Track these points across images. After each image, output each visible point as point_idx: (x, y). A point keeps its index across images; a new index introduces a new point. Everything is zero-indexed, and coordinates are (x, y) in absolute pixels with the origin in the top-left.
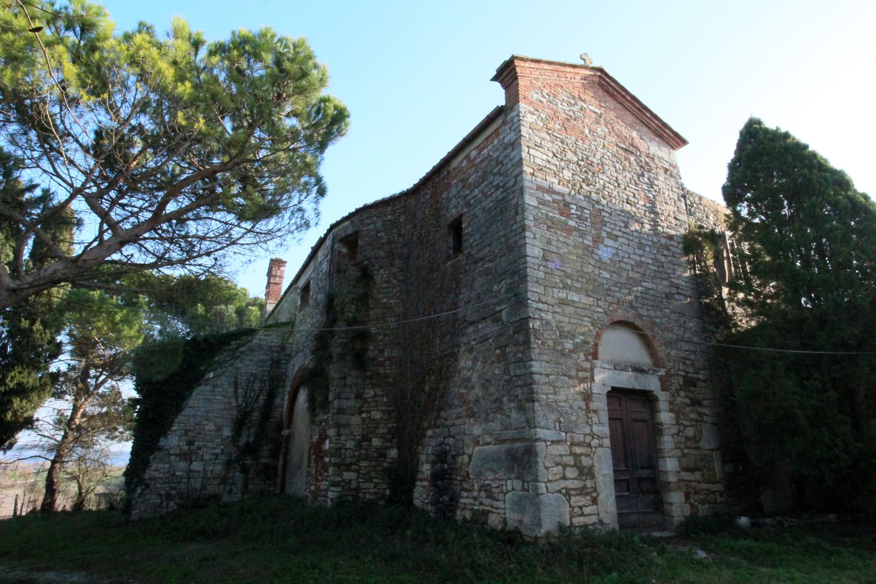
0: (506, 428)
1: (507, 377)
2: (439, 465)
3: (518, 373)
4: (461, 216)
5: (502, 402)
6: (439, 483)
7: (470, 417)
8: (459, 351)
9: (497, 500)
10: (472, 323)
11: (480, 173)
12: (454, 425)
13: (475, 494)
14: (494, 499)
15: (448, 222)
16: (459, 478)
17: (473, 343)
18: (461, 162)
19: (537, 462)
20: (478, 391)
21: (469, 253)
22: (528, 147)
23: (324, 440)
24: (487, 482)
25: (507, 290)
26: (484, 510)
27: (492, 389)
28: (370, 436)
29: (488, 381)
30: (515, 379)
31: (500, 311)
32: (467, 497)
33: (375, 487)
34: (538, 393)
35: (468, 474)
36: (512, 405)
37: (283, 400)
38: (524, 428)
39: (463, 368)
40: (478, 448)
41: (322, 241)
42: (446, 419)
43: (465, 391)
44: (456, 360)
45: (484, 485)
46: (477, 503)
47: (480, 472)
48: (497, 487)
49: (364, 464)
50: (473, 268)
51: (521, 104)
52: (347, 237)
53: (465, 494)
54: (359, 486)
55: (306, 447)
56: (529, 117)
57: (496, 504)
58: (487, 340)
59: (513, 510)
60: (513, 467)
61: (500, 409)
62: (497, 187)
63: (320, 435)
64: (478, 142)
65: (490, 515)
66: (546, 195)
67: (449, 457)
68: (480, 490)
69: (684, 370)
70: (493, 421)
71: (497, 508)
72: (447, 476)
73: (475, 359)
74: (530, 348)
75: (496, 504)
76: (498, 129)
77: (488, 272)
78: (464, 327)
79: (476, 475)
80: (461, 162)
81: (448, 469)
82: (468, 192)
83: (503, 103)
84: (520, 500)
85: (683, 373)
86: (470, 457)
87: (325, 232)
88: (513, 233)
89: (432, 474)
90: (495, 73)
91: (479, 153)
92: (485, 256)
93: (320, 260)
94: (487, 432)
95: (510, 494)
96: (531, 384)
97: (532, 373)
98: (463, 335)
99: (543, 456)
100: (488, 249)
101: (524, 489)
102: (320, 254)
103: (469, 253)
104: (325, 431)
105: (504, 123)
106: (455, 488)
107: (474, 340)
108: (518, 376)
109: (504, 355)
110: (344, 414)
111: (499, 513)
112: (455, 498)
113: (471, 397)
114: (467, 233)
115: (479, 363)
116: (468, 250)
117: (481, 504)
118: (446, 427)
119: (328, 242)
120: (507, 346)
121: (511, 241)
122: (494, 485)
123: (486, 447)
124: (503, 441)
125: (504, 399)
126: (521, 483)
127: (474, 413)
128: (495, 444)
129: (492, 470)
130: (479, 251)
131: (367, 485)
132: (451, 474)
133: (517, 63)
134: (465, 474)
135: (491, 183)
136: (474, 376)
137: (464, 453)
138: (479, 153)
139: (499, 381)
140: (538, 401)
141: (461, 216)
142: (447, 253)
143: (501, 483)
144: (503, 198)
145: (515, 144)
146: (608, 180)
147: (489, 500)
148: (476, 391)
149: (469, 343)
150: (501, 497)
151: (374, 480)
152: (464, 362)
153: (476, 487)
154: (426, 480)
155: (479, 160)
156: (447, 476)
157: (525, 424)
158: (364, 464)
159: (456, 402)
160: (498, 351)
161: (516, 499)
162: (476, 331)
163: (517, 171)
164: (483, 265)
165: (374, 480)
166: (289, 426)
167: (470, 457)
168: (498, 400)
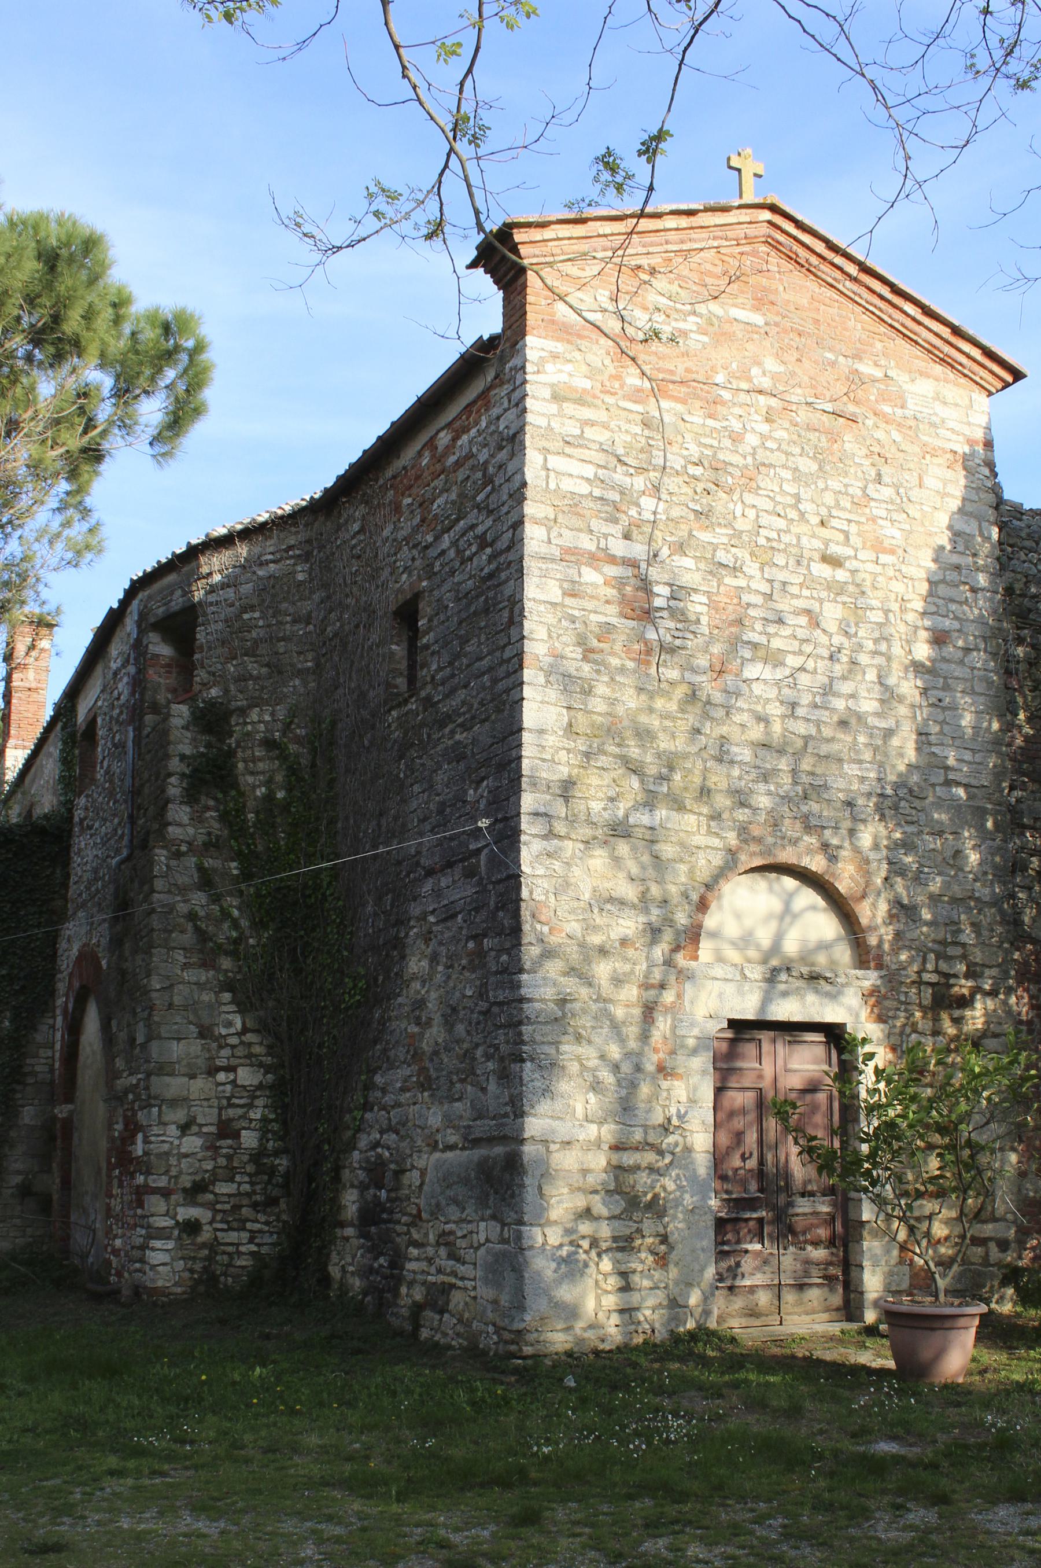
0: (480, 1117)
1: (483, 1005)
2: (372, 1191)
3: (501, 998)
4: (417, 596)
5: (474, 1059)
6: (373, 1229)
7: (422, 1087)
8: (407, 935)
9: (464, 1263)
10: (430, 873)
11: (453, 496)
12: (398, 1105)
13: (430, 1251)
14: (458, 1260)
15: (393, 607)
16: (404, 1219)
17: (432, 919)
18: (420, 454)
19: (522, 1186)
20: (436, 1033)
21: (428, 699)
22: (545, 451)
23: (133, 1136)
24: (448, 1227)
25: (489, 803)
26: (443, 1283)
27: (460, 1028)
28: (236, 1125)
29: (454, 1010)
30: (495, 1009)
31: (479, 851)
32: (417, 1259)
33: (251, 1241)
34: (534, 1042)
35: (419, 1211)
36: (491, 1065)
37: (53, 1027)
38: (506, 1115)
39: (414, 977)
40: (437, 1155)
41: (114, 619)
42: (384, 1091)
43: (416, 1030)
44: (403, 957)
45: (444, 1233)
46: (433, 1270)
47: (438, 1205)
48: (464, 1237)
49: (224, 1188)
50: (435, 737)
51: (529, 339)
52: (170, 617)
53: (414, 1252)
54: (216, 1238)
55: (104, 1144)
56: (548, 364)
57: (462, 1269)
58: (454, 916)
59: (486, 1281)
60: (488, 1195)
61: (469, 1074)
62: (483, 542)
63: (126, 1125)
64: (453, 411)
65: (453, 1292)
66: (585, 570)
67: (389, 1175)
68: (438, 1244)
69: (936, 971)
70: (459, 1099)
71: (462, 1279)
72: (385, 1216)
73: (434, 959)
74: (520, 945)
75: (462, 1269)
76: (489, 389)
77: (457, 754)
78: (415, 880)
79: (432, 1214)
80: (420, 454)
81: (389, 1199)
82: (430, 538)
83: (499, 330)
84: (497, 1261)
85: (933, 978)
86: (423, 1173)
87: (121, 595)
88: (504, 667)
89: (360, 1210)
90: (475, 253)
91: (454, 440)
92: (456, 712)
93: (114, 666)
94: (449, 1121)
95: (483, 1250)
96: (521, 1023)
97: (522, 1000)
98: (415, 899)
99: (538, 1173)
100: (462, 694)
101: (504, 1241)
102: (116, 649)
103: (428, 699)
104: (135, 1115)
105: (499, 380)
106: (398, 1240)
107: (433, 912)
108: (500, 1004)
109: (480, 953)
110: (172, 1074)
111: (466, 1289)
112: (397, 1262)
113: (426, 1046)
114: (427, 647)
115: (440, 968)
116: (429, 688)
117: (439, 1271)
118: (384, 1108)
119: (130, 624)
120: (485, 936)
121: (501, 686)
122: (459, 1234)
123: (449, 1155)
124: (476, 1143)
125: (479, 1052)
126: (498, 1229)
127: (428, 1078)
128: (463, 1149)
129: (456, 1202)
130: (447, 696)
131: (233, 1236)
132: (391, 1212)
133: (518, 236)
134: (414, 1212)
135: (473, 527)
136: (433, 995)
137: (413, 1167)
138: (454, 440)
139: (472, 1012)
140: (532, 1060)
141: (417, 596)
142: (388, 685)
143: (470, 1227)
144: (491, 576)
145: (513, 442)
146: (769, 505)
147: (451, 1263)
148: (435, 1030)
149: (425, 919)
150: (469, 1255)
151: (249, 1225)
152: (416, 965)
153: (432, 1238)
154: (352, 1225)
155: (452, 459)
156: (385, 1216)
157: (508, 1109)
158: (224, 1191)
159: (401, 1053)
160: (471, 945)
161: (490, 1259)
162: (437, 893)
163: (513, 518)
164: (453, 732)
165: (249, 1225)
166: (69, 1098)
167: (423, 1173)
168: (468, 1056)
